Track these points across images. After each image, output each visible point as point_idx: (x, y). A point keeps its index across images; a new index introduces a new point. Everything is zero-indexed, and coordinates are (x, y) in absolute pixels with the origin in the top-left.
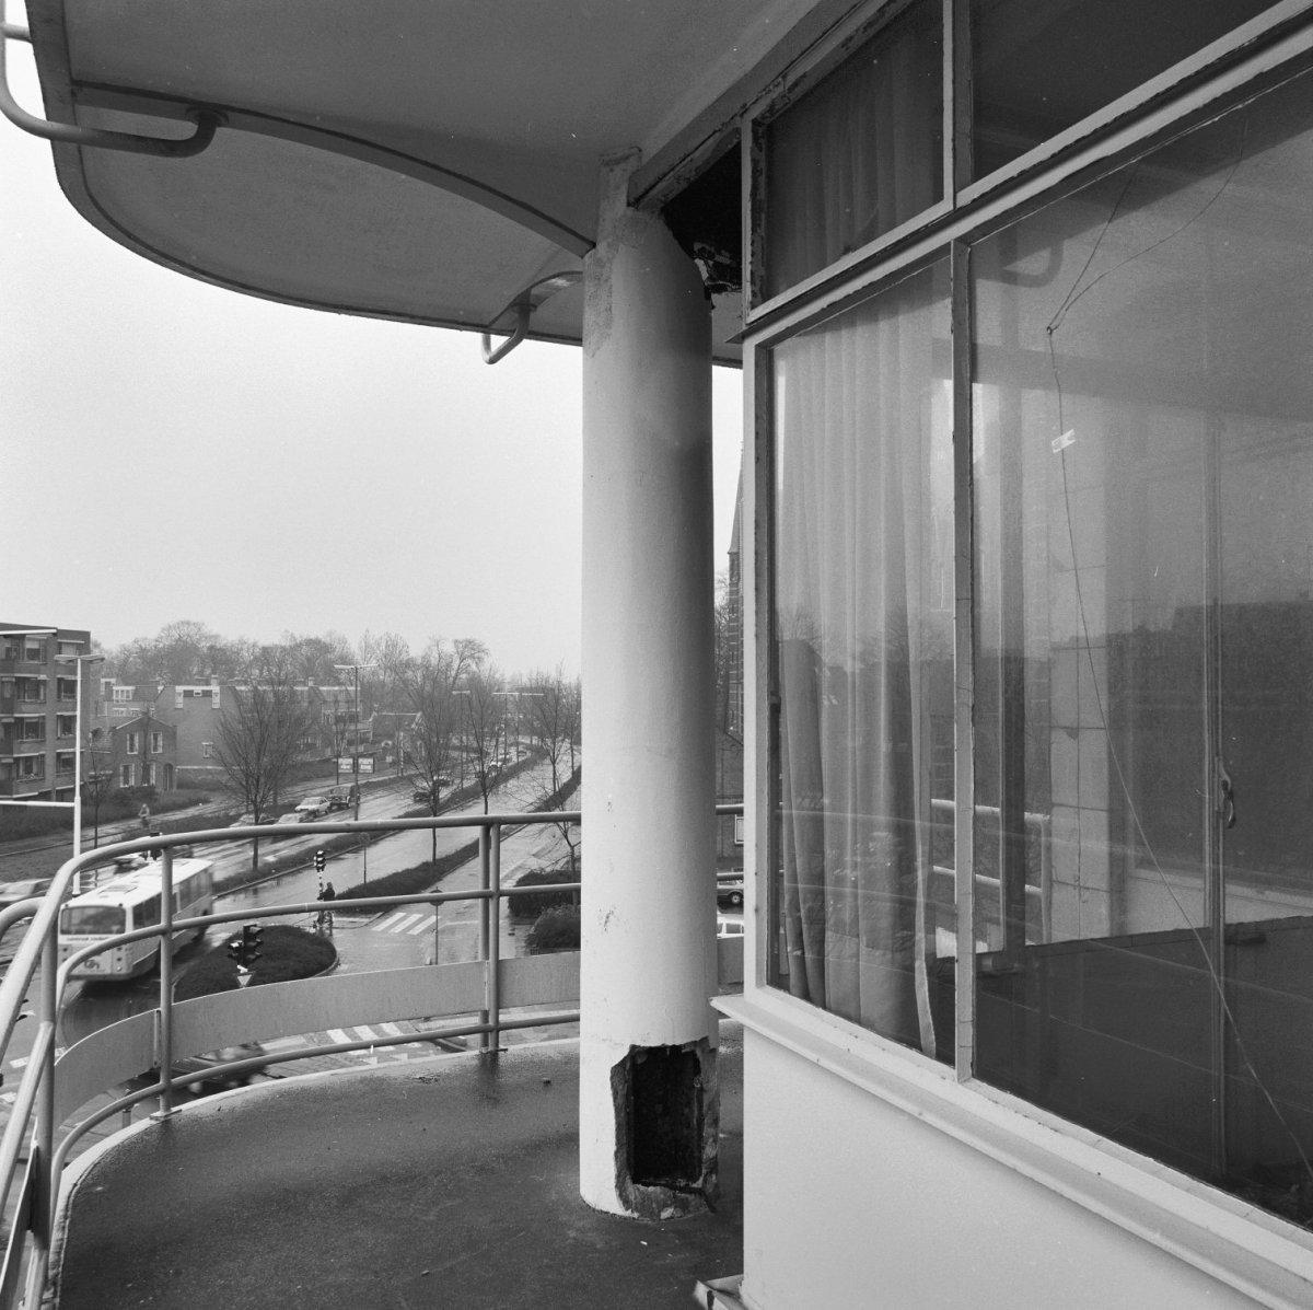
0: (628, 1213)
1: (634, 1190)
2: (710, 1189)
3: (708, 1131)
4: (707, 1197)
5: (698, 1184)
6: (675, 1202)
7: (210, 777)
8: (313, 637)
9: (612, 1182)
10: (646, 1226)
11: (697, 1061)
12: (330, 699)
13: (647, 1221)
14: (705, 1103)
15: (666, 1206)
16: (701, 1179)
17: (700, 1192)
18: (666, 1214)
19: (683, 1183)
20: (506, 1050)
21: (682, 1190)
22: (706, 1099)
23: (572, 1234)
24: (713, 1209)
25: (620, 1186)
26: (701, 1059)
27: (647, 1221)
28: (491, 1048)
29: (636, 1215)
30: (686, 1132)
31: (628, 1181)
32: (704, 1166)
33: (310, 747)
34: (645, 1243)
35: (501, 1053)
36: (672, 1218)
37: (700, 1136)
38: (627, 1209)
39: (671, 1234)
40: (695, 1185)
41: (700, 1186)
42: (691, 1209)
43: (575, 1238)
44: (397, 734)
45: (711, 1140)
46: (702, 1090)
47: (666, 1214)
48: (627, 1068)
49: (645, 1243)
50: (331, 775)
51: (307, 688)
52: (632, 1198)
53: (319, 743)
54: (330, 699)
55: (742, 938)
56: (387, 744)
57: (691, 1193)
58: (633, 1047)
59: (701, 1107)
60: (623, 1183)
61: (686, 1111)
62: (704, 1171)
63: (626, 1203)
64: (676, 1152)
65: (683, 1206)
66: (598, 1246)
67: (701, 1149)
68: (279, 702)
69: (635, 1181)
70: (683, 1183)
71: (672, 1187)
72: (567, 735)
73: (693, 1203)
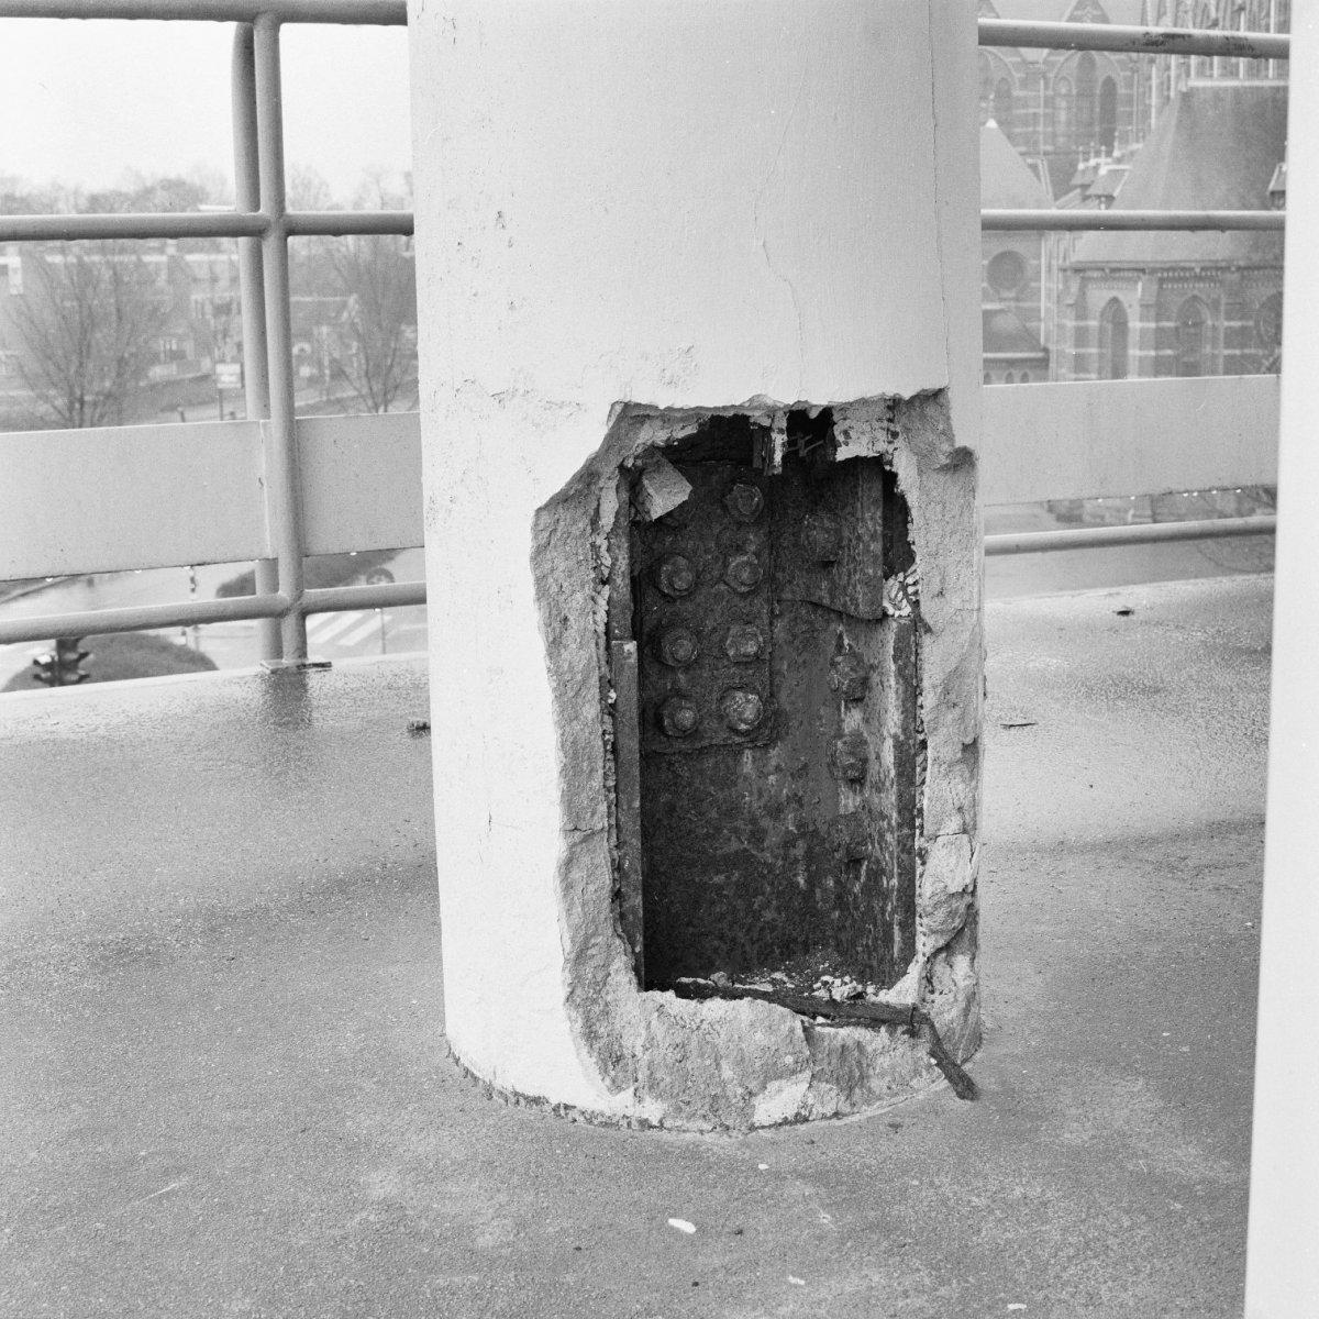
0: (621, 1104)
1: (650, 1017)
2: (945, 1012)
3: (938, 791)
4: (937, 1041)
5: (904, 992)
6: (813, 1059)
7: (16, 408)
8: (172, 176)
9: (555, 980)
10: (693, 1154)
11: (896, 510)
12: (203, 273)
13: (696, 1132)
14: (932, 676)
15: (774, 1072)
16: (915, 970)
17: (910, 1021)
18: (778, 1102)
19: (841, 989)
20: (324, 666)
21: (837, 1012)
22: (935, 660)
23: (382, 1184)
24: (965, 1087)
25: (587, 999)
26: (912, 499)
27: (696, 1132)
28: (288, 661)
29: (653, 1110)
30: (849, 801)
31: (622, 976)
32: (922, 925)
33: (177, 356)
34: (688, 1228)
35: (314, 679)
36: (800, 1119)
37: (910, 812)
38: (616, 1087)
39: (799, 1189)
40: (889, 997)
41: (910, 1000)
42: (877, 1084)
43: (387, 1205)
44: (315, 332)
45: (954, 824)
46: (917, 625)
47: (778, 1102)
48: (607, 520)
49: (688, 1228)
50: (213, 400)
51: (164, 259)
52: (634, 1042)
53: (189, 347)
54: (203, 273)
55: (985, 351)
56: (302, 350)
57: (874, 1023)
58: (630, 416)
59: (912, 691)
60: (600, 985)
61: (853, 719)
62: (925, 944)
63: (613, 1060)
64: (812, 881)
65: (850, 1076)
66: (485, 1241)
67: (911, 858)
68: (117, 280)
69: (653, 975)
70: (841, 989)
71: (805, 1007)
72: (629, 470)
73: (884, 1062)
